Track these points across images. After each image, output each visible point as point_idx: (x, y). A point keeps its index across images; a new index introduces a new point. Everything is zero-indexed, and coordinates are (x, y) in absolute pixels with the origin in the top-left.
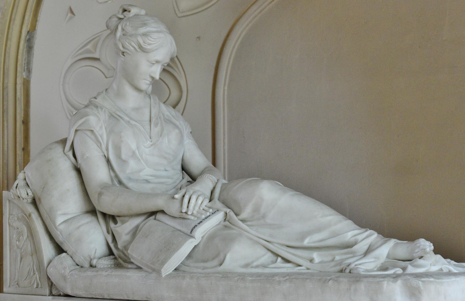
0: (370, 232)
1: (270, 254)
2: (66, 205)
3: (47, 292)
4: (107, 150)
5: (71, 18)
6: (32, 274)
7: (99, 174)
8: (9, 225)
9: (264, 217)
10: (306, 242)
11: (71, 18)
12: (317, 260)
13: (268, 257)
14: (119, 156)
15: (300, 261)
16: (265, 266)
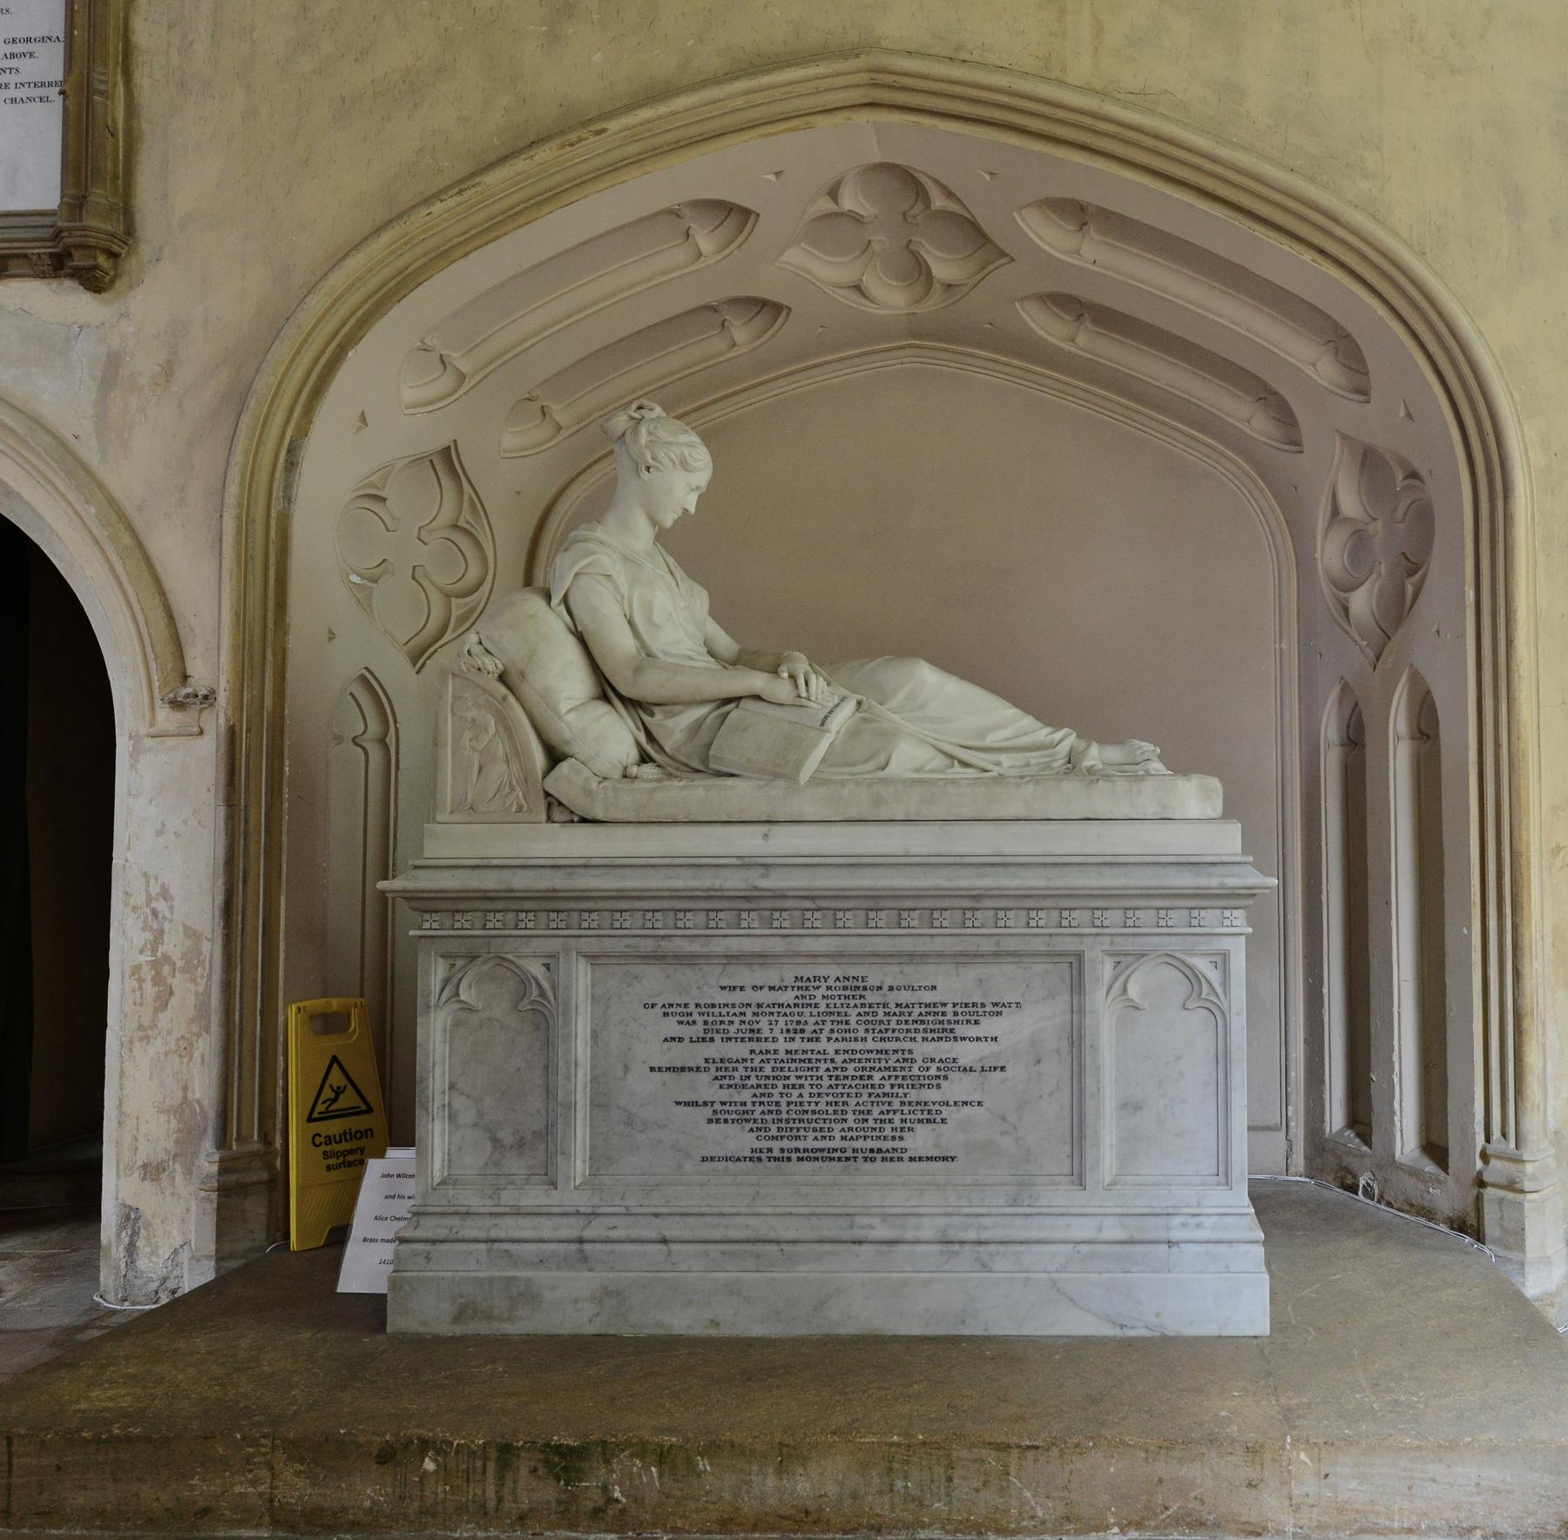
0: (1066, 730)
1: (940, 756)
2: (564, 681)
3: (544, 817)
4: (631, 607)
5: (359, 429)
6: (507, 790)
7: (619, 644)
8: (453, 714)
9: (922, 707)
10: (990, 741)
11: (359, 429)
12: (1006, 764)
13: (944, 761)
14: (649, 619)
15: (989, 766)
16: (941, 771)
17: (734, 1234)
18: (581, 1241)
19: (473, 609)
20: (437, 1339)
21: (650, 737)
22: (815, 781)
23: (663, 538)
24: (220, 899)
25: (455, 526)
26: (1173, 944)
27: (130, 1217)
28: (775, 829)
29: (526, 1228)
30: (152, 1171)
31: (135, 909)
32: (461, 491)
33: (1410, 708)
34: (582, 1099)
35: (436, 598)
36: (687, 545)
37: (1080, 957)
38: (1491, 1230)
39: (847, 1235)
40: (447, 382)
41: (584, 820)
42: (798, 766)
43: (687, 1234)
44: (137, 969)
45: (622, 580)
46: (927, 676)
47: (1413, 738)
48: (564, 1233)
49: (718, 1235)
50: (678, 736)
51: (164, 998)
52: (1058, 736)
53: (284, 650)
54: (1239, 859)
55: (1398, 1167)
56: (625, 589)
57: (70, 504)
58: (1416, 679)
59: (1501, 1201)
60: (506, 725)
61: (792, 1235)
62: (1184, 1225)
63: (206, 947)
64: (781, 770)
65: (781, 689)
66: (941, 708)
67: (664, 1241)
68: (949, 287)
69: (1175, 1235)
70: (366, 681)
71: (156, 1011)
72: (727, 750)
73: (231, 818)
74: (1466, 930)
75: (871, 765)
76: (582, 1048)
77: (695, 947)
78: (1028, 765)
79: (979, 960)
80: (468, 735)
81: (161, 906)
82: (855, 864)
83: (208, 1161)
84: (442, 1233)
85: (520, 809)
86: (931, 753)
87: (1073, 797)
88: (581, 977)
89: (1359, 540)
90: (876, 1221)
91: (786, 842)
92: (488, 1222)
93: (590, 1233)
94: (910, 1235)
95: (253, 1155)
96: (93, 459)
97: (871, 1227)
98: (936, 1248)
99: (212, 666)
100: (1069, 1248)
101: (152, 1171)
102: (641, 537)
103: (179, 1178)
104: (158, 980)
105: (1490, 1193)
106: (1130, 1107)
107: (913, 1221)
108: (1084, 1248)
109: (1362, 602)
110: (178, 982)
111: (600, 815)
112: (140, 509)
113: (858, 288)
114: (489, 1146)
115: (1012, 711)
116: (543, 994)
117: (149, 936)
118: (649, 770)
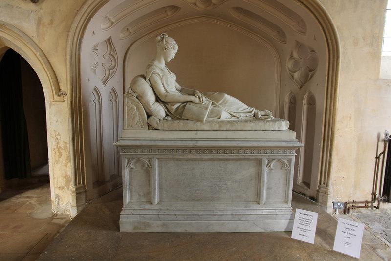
2: (151, 97)
10: (239, 111)
12: (242, 116)
17: (190, 214)
18: (158, 215)
19: (114, 72)
20: (131, 233)
21: (168, 110)
22: (207, 122)
23: (167, 64)
24: (71, 137)
25: (110, 54)
26: (281, 158)
27: (57, 197)
28: (199, 132)
29: (147, 212)
30: (61, 188)
31: (53, 137)
32: (111, 47)
33: (307, 99)
34: (157, 187)
35: (107, 70)
36: (171, 66)
37: (262, 159)
38: (320, 199)
39: (213, 214)
40: (109, 24)
41: (156, 129)
42: (203, 118)
43: (180, 214)
44: (54, 149)
45: (161, 75)
46: (227, 96)
47: (308, 104)
48: (155, 214)
49: (186, 214)
50: (174, 110)
51: (60, 155)
52: (252, 109)
53: (80, 84)
54: (294, 140)
55: (298, 185)
56: (162, 77)
57: (33, 52)
58: (310, 93)
59: (323, 196)
60: (138, 108)
61: (201, 214)
62: (279, 211)
63: (68, 145)
64: (199, 120)
65: (197, 100)
66: (232, 107)
67: (176, 215)
68: (214, 4)
69: (277, 213)
70: (96, 89)
71: (59, 158)
72: (186, 114)
73: (73, 120)
74: (319, 145)
75: (217, 118)
76: (157, 177)
77: (181, 157)
78: (246, 116)
79: (234, 155)
80: (130, 111)
81: (58, 137)
82: (216, 140)
83: (72, 187)
84: (130, 213)
85: (142, 127)
86: (228, 114)
87: (260, 125)
88: (156, 163)
89: (296, 63)
90: (218, 211)
91: (200, 135)
92: (139, 211)
93: (160, 214)
94: (225, 214)
95: (81, 187)
96: (37, 42)
97: (217, 212)
98: (230, 216)
99: (66, 87)
100: (257, 216)
101: (61, 188)
102: (163, 65)
103: (66, 190)
104: (59, 151)
105: (320, 194)
106: (269, 188)
107: (225, 211)
108: (260, 216)
109: (296, 75)
110: (63, 152)
111: (160, 129)
112: (48, 53)
113: (195, 4)
114: (138, 196)
115: (243, 104)
116: (148, 166)
117: (56, 143)
118: (169, 118)
